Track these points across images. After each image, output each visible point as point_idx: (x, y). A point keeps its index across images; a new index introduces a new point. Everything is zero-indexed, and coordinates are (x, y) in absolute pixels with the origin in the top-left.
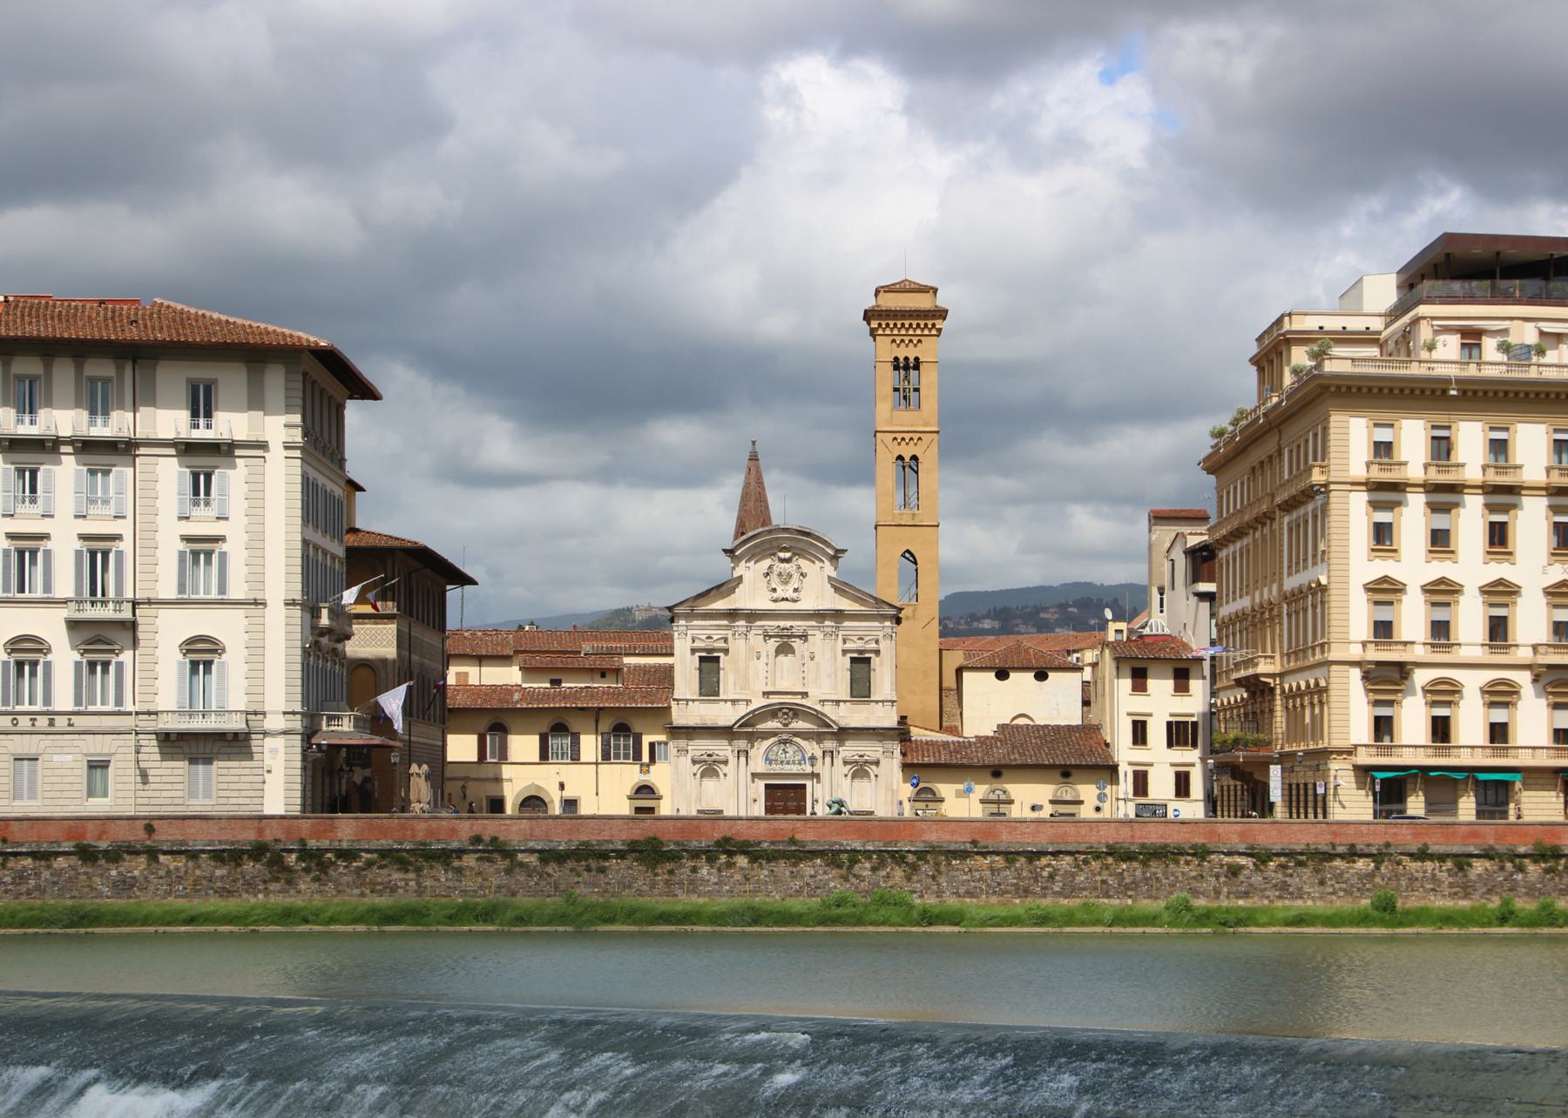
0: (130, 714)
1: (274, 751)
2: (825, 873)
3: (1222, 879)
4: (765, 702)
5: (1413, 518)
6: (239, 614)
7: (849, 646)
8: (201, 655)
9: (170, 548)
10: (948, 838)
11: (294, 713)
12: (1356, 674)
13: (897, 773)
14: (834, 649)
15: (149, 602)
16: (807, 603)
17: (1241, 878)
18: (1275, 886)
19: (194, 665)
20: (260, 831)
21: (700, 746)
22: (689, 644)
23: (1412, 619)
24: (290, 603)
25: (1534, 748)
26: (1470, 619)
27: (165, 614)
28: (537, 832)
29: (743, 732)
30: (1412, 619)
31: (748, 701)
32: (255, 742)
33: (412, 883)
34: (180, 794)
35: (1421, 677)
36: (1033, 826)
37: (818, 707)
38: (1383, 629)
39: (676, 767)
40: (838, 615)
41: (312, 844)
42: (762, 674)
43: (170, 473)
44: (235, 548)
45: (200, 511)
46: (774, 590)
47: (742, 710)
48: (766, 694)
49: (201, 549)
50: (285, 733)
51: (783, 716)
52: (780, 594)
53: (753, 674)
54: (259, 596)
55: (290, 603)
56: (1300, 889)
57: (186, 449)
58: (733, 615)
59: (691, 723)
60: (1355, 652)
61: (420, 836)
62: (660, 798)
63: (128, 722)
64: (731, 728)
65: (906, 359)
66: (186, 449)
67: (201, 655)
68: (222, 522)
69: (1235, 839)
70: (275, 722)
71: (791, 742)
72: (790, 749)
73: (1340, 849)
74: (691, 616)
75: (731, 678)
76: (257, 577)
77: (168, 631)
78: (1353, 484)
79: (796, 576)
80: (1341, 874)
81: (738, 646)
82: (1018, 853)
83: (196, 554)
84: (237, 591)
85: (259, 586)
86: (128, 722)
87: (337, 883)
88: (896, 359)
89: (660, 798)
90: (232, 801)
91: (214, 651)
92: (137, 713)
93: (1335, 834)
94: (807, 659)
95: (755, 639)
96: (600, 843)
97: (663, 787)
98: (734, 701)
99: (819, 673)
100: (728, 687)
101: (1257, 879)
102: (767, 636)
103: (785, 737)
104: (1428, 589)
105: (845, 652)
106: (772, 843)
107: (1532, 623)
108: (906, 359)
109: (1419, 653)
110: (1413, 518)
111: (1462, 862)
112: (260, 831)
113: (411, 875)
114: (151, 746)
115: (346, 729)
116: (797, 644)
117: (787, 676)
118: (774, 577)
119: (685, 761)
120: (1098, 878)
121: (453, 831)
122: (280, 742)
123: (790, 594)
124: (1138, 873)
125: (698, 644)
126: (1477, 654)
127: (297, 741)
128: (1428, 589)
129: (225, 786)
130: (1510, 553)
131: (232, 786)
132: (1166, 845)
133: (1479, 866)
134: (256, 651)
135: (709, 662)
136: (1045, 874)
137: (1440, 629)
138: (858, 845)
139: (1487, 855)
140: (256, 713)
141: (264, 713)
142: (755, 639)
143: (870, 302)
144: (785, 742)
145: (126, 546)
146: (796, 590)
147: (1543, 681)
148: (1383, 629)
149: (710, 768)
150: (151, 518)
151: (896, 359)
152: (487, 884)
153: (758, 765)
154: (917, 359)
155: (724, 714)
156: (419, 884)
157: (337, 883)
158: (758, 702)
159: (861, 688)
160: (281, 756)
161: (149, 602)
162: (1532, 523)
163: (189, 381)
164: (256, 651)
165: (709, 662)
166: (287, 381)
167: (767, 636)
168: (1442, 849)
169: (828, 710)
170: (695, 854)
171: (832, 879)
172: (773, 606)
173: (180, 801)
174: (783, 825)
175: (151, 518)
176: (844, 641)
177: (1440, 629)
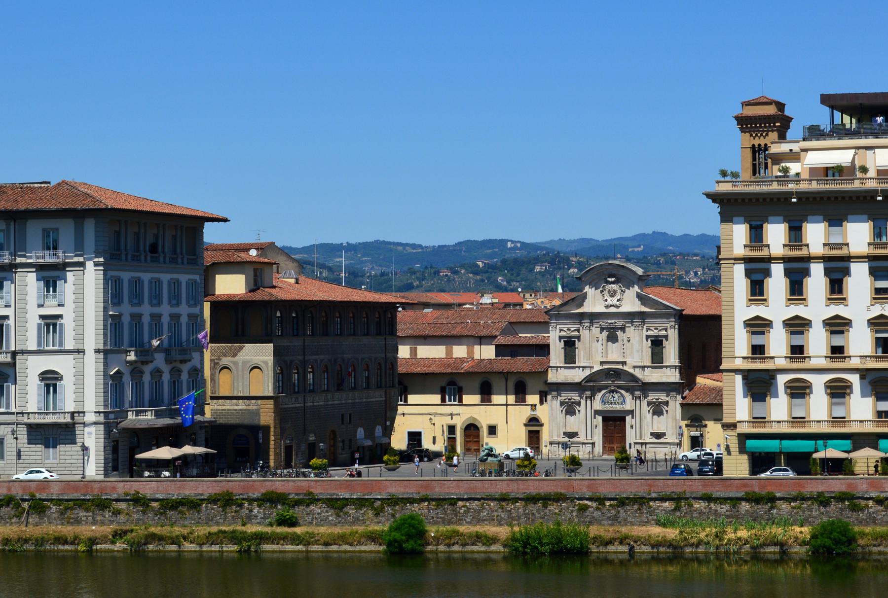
0: (13, 413)
1: (90, 433)
2: (327, 512)
3: (575, 514)
4: (601, 368)
5: (777, 282)
6: (70, 357)
7: (650, 333)
8: (50, 380)
9: (33, 322)
10: (402, 490)
11: (99, 412)
12: (739, 378)
13: (679, 410)
14: (641, 336)
15: (23, 352)
16: (626, 308)
17: (587, 513)
18: (609, 518)
19: (48, 386)
20: (9, 489)
21: (565, 396)
22: (558, 333)
23: (778, 343)
24: (97, 351)
25: (861, 421)
26: (817, 342)
27: (31, 358)
28: (161, 488)
29: (589, 386)
30: (778, 343)
31: (591, 367)
32: (79, 429)
33: (90, 518)
34: (40, 457)
35: (782, 380)
36: (455, 483)
37: (631, 371)
38: (758, 350)
39: (551, 406)
40: (642, 316)
41: (38, 496)
42: (600, 351)
43: (30, 281)
44: (68, 322)
45: (51, 301)
46: (606, 300)
47: (587, 372)
48: (602, 363)
49: (51, 323)
50: (95, 423)
51: (613, 378)
52: (609, 302)
53: (595, 352)
54: (80, 347)
55: (97, 351)
56: (625, 520)
57: (40, 268)
58: (582, 316)
59: (559, 381)
60: (739, 364)
61: (96, 492)
62: (542, 425)
63: (11, 418)
64: (580, 383)
65: (760, 145)
66: (40, 268)
67: (50, 380)
68: (61, 308)
69: (585, 490)
70: (90, 418)
71: (617, 392)
72: (616, 396)
73: (654, 495)
74: (558, 317)
75: (582, 353)
76: (80, 335)
77: (32, 368)
78: (735, 259)
79: (619, 292)
80: (653, 511)
81: (585, 334)
82: (444, 499)
83: (48, 325)
84: (69, 345)
85: (81, 341)
86: (11, 418)
87: (49, 518)
88: (754, 145)
89: (542, 425)
90: (68, 461)
91: (57, 379)
92: (18, 413)
93: (650, 485)
94: (625, 342)
95: (596, 330)
96: (196, 495)
97: (544, 419)
98: (584, 368)
99: (632, 352)
100: (581, 360)
101: (597, 514)
102: (602, 329)
103: (613, 388)
104: (788, 324)
105: (648, 337)
106: (297, 494)
107: (861, 343)
108: (760, 145)
109: (781, 363)
110: (777, 282)
111: (735, 501)
112: (9, 489)
113: (90, 514)
114: (22, 432)
115: (149, 417)
116: (619, 333)
117: (614, 353)
118: (606, 293)
119: (556, 404)
120: (495, 514)
121: (114, 488)
122: (92, 429)
123: (615, 302)
124: (521, 510)
125: (563, 333)
126: (822, 363)
127: (102, 427)
128: (788, 324)
129: (63, 453)
130: (844, 299)
131: (67, 453)
132: (539, 494)
133: (745, 506)
134: (80, 378)
135: (570, 344)
136: (462, 511)
137: (797, 351)
138: (347, 496)
139: (747, 500)
140: (79, 413)
141: (84, 413)
142: (596, 330)
143: (739, 111)
144: (613, 391)
145: (11, 322)
146: (618, 300)
147: (868, 380)
148: (758, 350)
149: (570, 409)
150: (24, 306)
151: (754, 145)
152: (131, 518)
153: (598, 405)
154: (766, 145)
155: (577, 376)
156: (94, 518)
157: (49, 518)
158: (597, 368)
159: (657, 357)
160: (93, 436)
161: (23, 352)
162: (859, 279)
163: (44, 230)
164: (80, 378)
165: (570, 344)
166: (96, 227)
167: (602, 329)
168: (723, 495)
169: (638, 373)
170: (251, 501)
171: (332, 515)
172: (604, 310)
173: (40, 461)
174: (303, 484)
175: (24, 306)
176: (648, 330)
177: (797, 351)
